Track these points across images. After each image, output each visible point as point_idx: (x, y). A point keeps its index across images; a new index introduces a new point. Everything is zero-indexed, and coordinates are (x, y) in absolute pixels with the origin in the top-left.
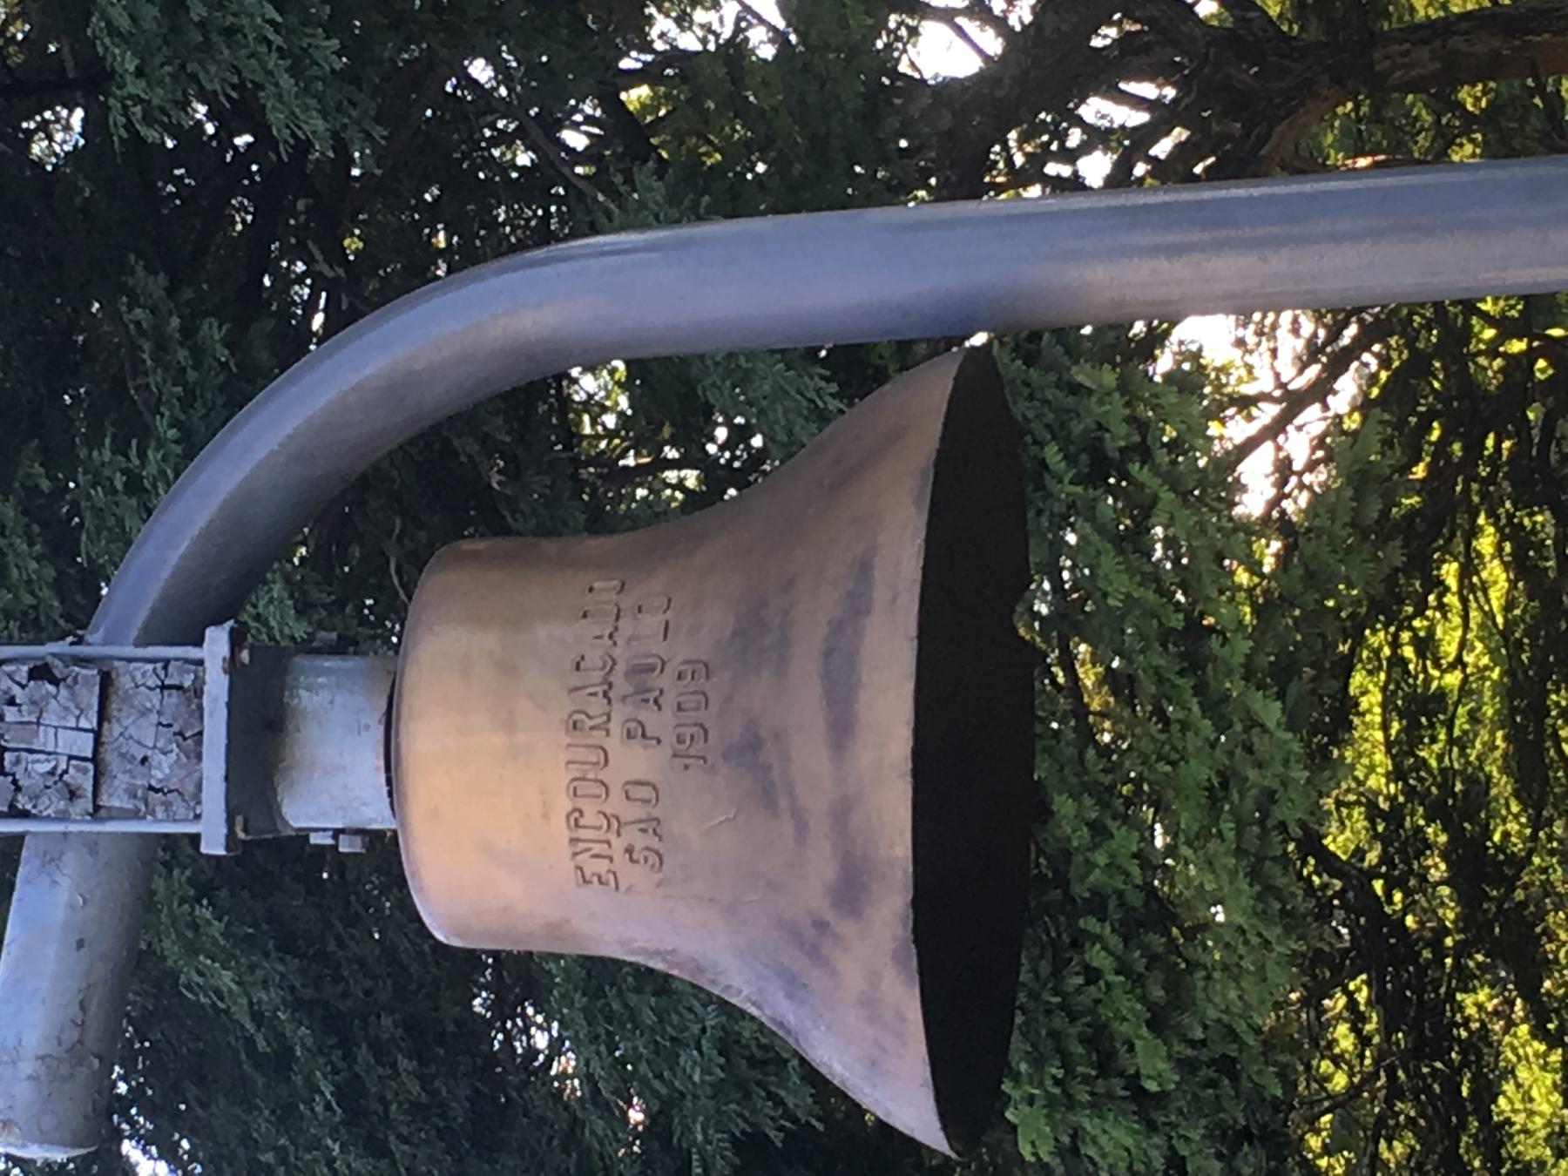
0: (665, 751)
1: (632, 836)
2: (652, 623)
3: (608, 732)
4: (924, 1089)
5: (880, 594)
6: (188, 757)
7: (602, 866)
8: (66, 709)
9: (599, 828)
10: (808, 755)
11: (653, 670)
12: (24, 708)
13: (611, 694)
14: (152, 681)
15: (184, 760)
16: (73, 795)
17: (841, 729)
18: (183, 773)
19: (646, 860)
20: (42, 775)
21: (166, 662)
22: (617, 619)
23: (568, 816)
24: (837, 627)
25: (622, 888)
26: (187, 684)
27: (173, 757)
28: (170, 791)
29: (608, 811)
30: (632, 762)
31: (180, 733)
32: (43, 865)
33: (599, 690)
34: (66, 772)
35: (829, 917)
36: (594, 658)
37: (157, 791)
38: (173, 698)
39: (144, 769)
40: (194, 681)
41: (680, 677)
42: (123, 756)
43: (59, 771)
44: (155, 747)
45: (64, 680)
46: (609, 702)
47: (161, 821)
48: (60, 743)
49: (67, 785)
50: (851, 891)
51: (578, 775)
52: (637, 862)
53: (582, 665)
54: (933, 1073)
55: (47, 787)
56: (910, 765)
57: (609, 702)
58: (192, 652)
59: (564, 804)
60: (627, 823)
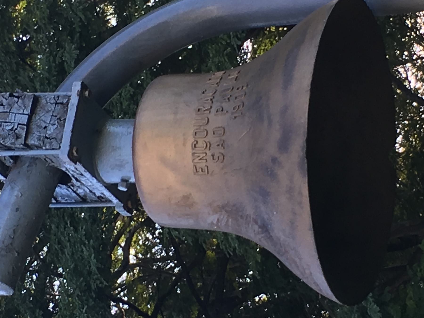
6: (60, 126)
7: (203, 164)
8: (20, 107)
12: (6, 107)
13: (213, 100)
14: (53, 101)
16: (18, 137)
18: (58, 132)
20: (8, 130)
25: (210, 173)
27: (56, 126)
28: (53, 138)
29: (207, 141)
30: (217, 121)
31: (59, 119)
32: (10, 183)
33: (209, 99)
34: (16, 129)
37: (48, 138)
38: (59, 107)
39: (44, 131)
40: (67, 101)
42: (38, 126)
43: (14, 129)
44: (50, 123)
45: (21, 97)
46: (212, 102)
48: (16, 119)
49: (16, 134)
50: (284, 145)
53: (205, 93)
55: (9, 134)
56: (310, 88)
57: (212, 102)
59: (191, 140)
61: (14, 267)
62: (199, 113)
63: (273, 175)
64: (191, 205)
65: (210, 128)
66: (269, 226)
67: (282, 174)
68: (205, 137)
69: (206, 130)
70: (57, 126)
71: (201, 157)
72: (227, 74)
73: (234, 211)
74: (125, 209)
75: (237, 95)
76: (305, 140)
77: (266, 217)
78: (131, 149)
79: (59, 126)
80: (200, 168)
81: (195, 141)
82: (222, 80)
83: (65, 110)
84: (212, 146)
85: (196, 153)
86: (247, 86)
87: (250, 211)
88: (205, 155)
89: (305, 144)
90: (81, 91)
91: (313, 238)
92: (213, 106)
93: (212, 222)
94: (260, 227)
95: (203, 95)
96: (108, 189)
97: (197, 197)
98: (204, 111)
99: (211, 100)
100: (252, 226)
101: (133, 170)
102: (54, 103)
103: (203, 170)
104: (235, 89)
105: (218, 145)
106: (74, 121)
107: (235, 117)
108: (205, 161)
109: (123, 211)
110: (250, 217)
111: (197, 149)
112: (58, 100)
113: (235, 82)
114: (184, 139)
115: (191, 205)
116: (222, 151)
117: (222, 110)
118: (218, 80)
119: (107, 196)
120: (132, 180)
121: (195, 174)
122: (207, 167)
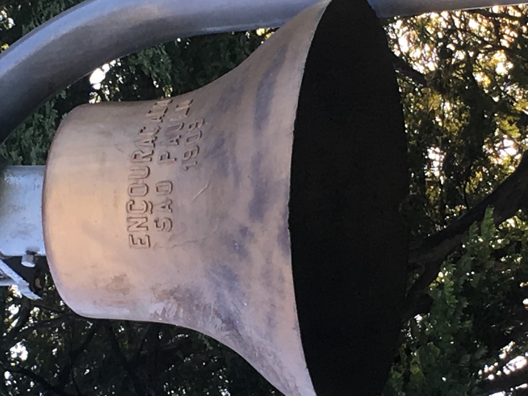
4: (295, 331)
7: (142, 233)
13: (155, 142)
22: (165, 112)
30: (162, 172)
33: (150, 140)
35: (248, 224)
46: (154, 145)
50: (258, 209)
53: (144, 130)
54: (299, 317)
57: (154, 145)
59: (125, 198)
62: (136, 160)
63: (242, 252)
64: (125, 291)
65: (152, 182)
66: (238, 322)
67: (256, 252)
68: (145, 195)
69: (146, 185)
71: (140, 223)
72: (175, 104)
73: (186, 298)
74: (31, 290)
75: (189, 135)
76: (287, 204)
77: (232, 308)
78: (41, 209)
81: (131, 200)
82: (167, 113)
84: (154, 208)
85: (133, 218)
86: (204, 123)
87: (209, 298)
88: (145, 220)
89: (288, 209)
91: (300, 338)
92: (155, 151)
93: (156, 312)
94: (223, 321)
95: (142, 134)
96: (7, 264)
97: (134, 278)
98: (144, 157)
99: (153, 142)
100: (212, 319)
101: (43, 238)
103: (143, 242)
104: (187, 126)
105: (164, 207)
107: (187, 168)
108: (146, 229)
109: (29, 293)
110: (210, 307)
111: (132, 212)
113: (186, 116)
114: (115, 197)
115: (125, 291)
116: (170, 215)
117: (169, 157)
118: (163, 113)
119: (6, 273)
120: (42, 252)
121: (131, 246)
122: (149, 237)
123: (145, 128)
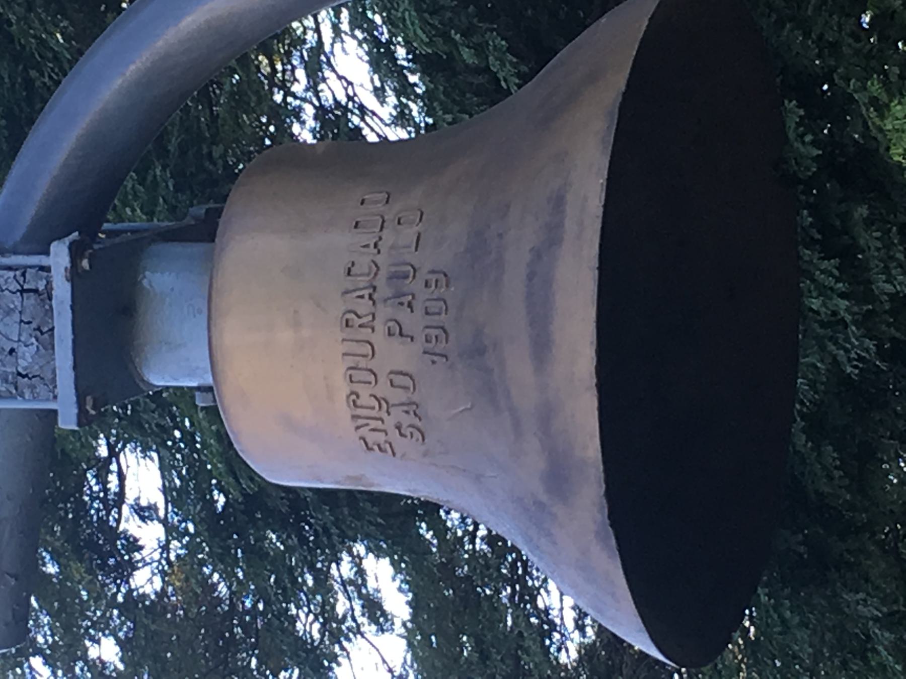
0: (419, 346)
1: (398, 414)
2: (409, 234)
3: (373, 330)
5: (570, 225)
9: (373, 408)
10: (518, 365)
11: (407, 277)
13: (375, 296)
14: (14, 286)
15: (43, 351)
17: (542, 346)
19: (412, 434)
21: (24, 270)
22: (381, 229)
23: (348, 397)
24: (537, 254)
25: (398, 455)
26: (41, 288)
28: (34, 377)
30: (396, 355)
31: (38, 329)
33: (366, 292)
36: (363, 264)
37: (24, 376)
38: (31, 300)
40: (46, 286)
41: (427, 284)
44: (19, 340)
46: (374, 303)
47: (29, 400)
51: (353, 365)
52: (405, 436)
56: (595, 381)
58: (43, 260)
59: (344, 389)
60: (393, 405)
61: (15, 606)
70: (38, 347)
79: (41, 348)
80: (374, 444)
83: (47, 307)
90: (72, 267)
94: (198, 368)
102: (18, 290)
106: (74, 341)
112: (24, 281)
123: (353, 264)
